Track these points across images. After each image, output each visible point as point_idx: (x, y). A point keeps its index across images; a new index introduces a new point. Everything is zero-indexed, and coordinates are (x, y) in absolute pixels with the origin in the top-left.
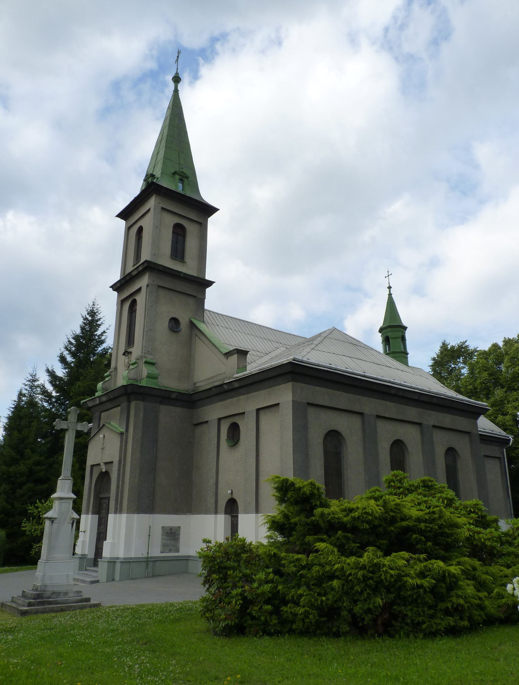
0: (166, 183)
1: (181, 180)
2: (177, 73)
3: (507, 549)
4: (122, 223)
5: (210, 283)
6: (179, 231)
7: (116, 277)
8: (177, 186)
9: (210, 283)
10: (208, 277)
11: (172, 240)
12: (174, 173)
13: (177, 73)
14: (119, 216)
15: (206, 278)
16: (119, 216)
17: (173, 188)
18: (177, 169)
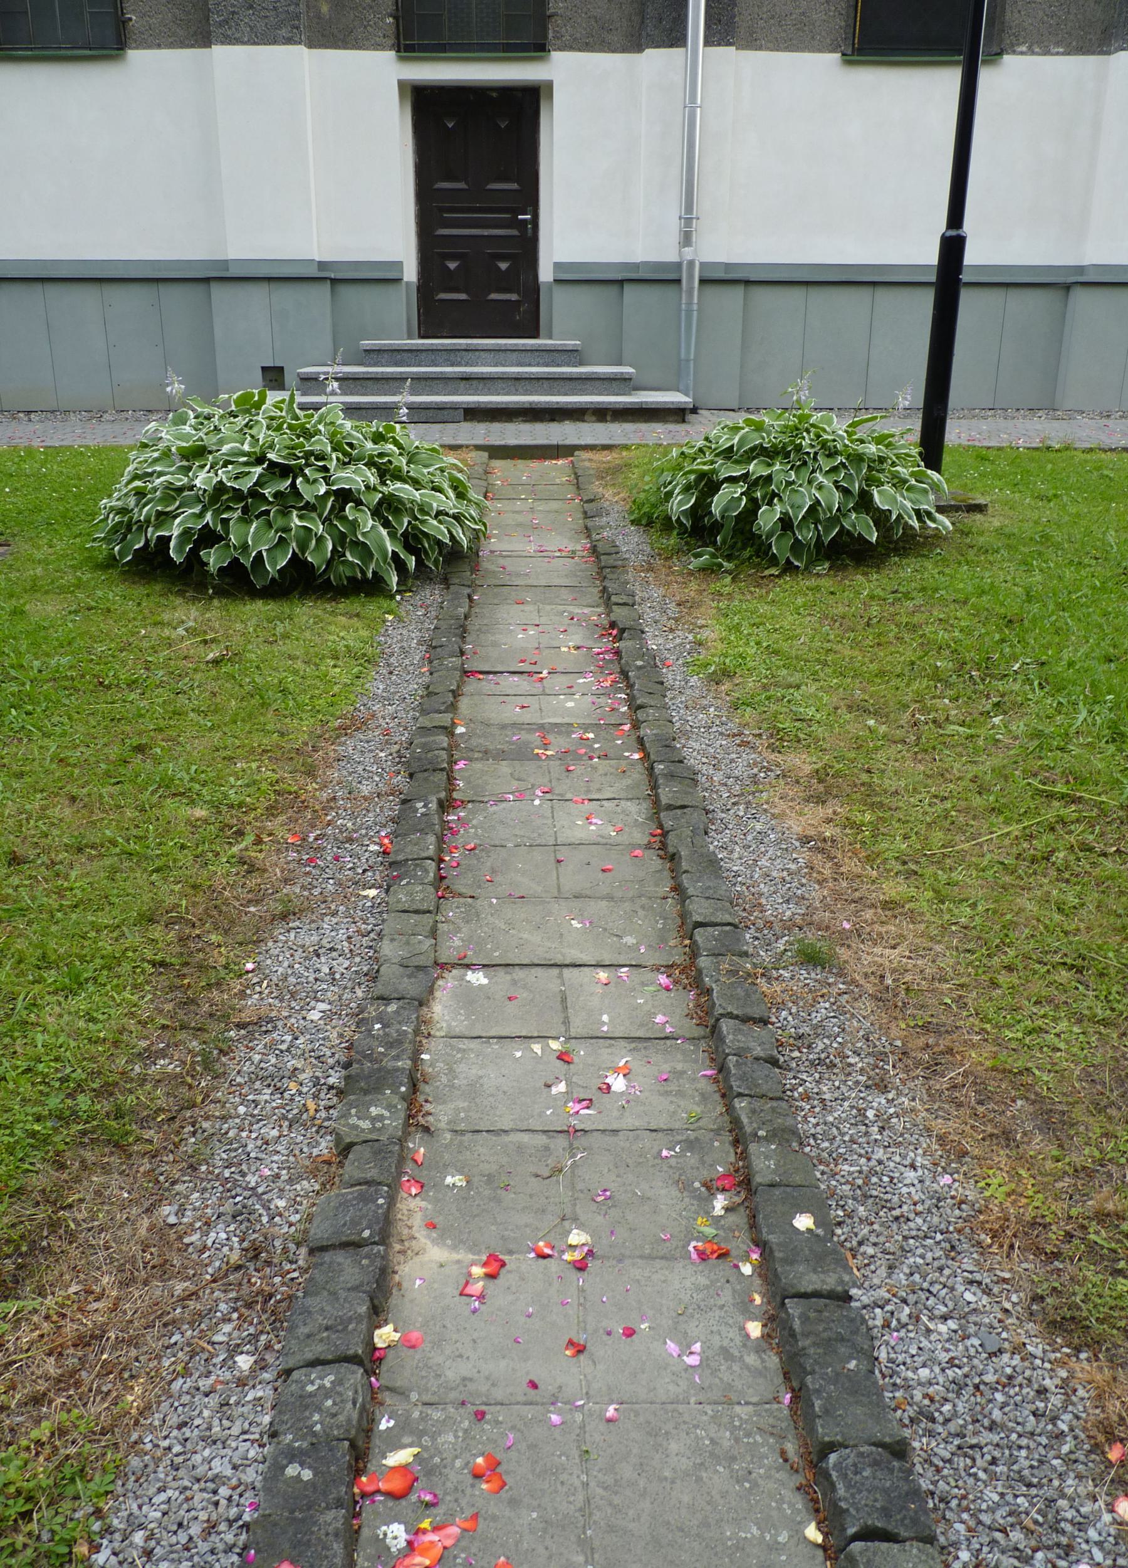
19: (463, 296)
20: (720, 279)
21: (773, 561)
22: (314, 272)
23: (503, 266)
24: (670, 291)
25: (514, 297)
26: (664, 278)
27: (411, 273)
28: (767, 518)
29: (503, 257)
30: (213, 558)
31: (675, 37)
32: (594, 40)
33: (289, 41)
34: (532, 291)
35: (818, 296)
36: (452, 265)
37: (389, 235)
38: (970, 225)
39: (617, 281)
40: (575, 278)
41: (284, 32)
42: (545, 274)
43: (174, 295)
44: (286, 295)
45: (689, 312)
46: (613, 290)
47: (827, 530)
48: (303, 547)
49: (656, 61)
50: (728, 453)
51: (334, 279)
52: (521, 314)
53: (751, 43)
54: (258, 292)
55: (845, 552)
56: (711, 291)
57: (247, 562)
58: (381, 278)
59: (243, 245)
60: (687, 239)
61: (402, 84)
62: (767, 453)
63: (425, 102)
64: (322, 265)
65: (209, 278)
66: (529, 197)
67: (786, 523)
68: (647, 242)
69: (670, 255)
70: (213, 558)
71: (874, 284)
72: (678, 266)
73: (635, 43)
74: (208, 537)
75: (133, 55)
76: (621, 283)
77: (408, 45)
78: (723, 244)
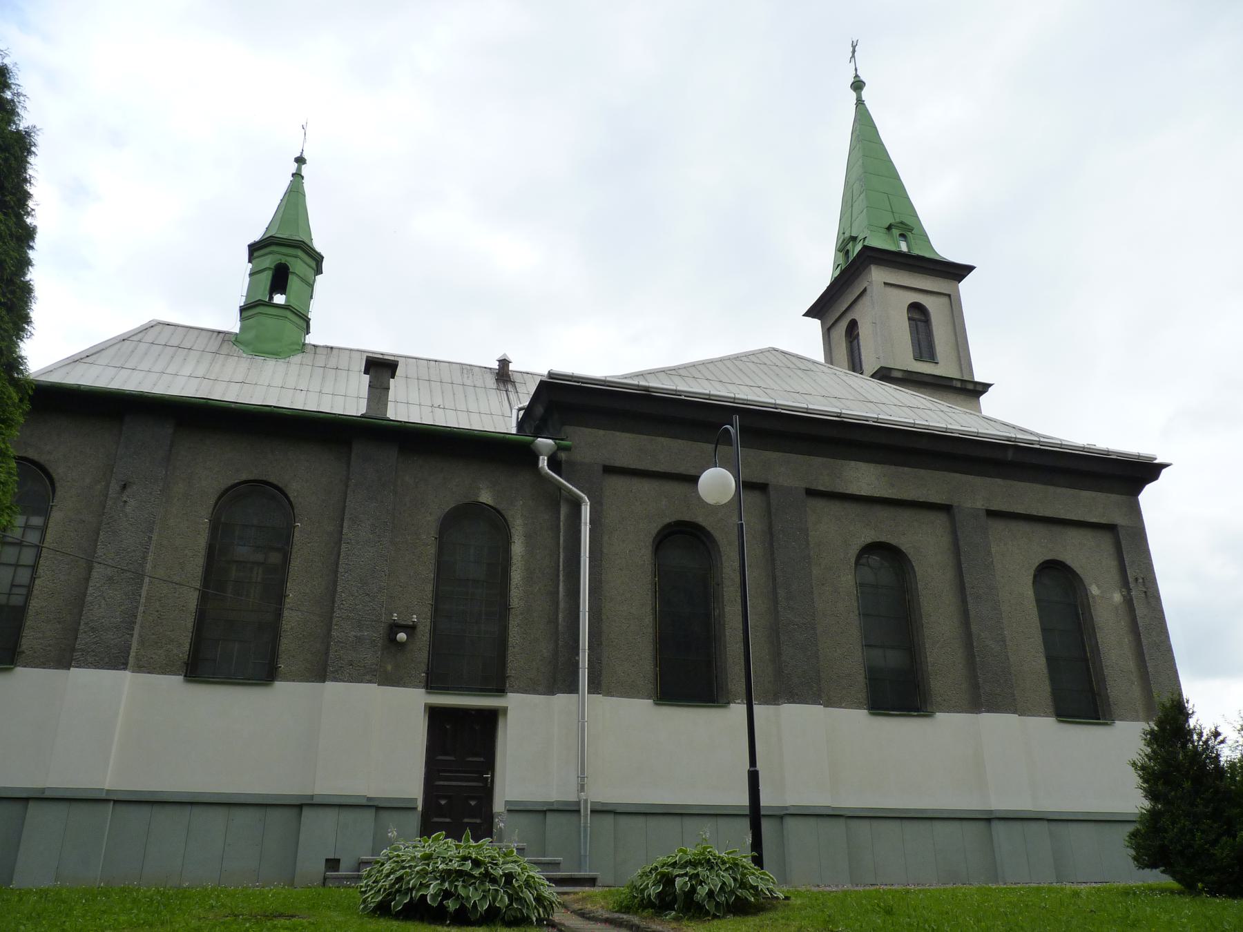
0: (879, 242)
1: (903, 236)
2: (857, 76)
3: (114, 487)
4: (816, 324)
5: (985, 387)
6: (918, 313)
7: (257, 236)
8: (899, 246)
9: (985, 387)
10: (979, 377)
11: (1045, 484)
12: (889, 228)
13: (857, 76)
14: (809, 313)
15: (976, 379)
16: (809, 313)
17: (892, 248)
18: (891, 221)
19: (448, 820)
20: (600, 811)
21: (707, 913)
22: (364, 802)
23: (473, 803)
24: (574, 817)
25: (478, 821)
26: (571, 810)
27: (420, 808)
28: (702, 891)
29: (473, 798)
30: (451, 905)
31: (572, 688)
32: (531, 688)
33: (370, 682)
34: (489, 817)
35: (653, 822)
36: (443, 802)
37: (408, 782)
38: (759, 766)
39: (542, 812)
40: (516, 810)
41: (368, 677)
42: (498, 806)
43: (275, 815)
44: (348, 816)
45: (585, 827)
46: (540, 817)
47: (730, 897)
48: (494, 899)
49: (561, 700)
50: (674, 865)
51: (377, 807)
52: (484, 827)
53: (609, 693)
54: (331, 814)
55: (741, 908)
56: (598, 817)
57: (469, 906)
58: (402, 807)
59: (326, 786)
60: (582, 788)
61: (426, 705)
62: (693, 864)
63: (435, 714)
64: (369, 799)
65: (300, 806)
66: (490, 765)
67: (711, 894)
68: (557, 790)
69: (572, 797)
70: (451, 905)
71: (681, 814)
72: (578, 803)
73: (551, 690)
74: (447, 895)
75: (277, 684)
76: (544, 812)
77: (432, 684)
78: (603, 792)
